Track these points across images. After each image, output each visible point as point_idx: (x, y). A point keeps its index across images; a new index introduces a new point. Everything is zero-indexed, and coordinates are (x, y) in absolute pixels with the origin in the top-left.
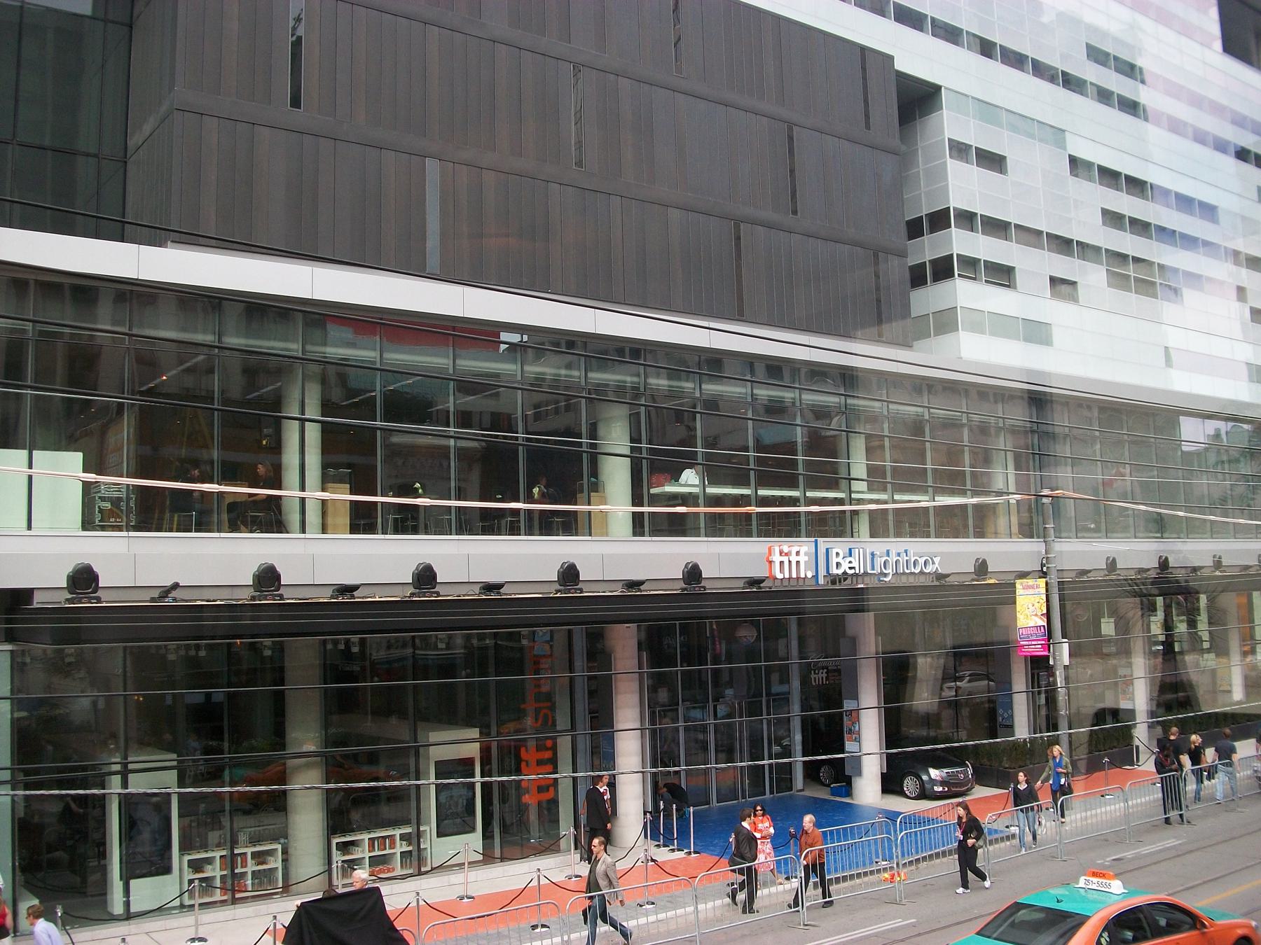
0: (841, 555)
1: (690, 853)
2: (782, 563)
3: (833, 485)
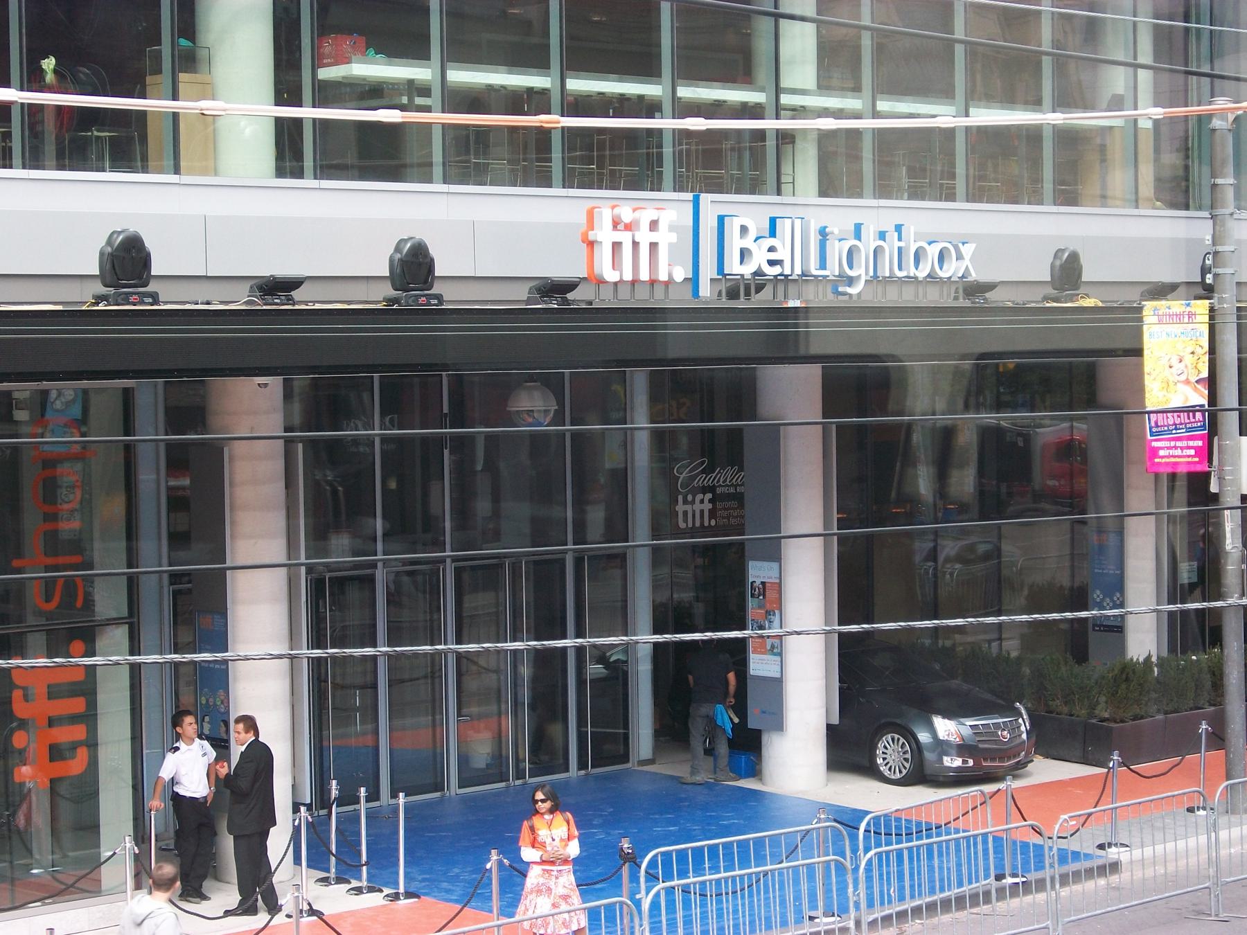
0: (752, 234)
1: (396, 897)
2: (616, 246)
3: (741, 73)
